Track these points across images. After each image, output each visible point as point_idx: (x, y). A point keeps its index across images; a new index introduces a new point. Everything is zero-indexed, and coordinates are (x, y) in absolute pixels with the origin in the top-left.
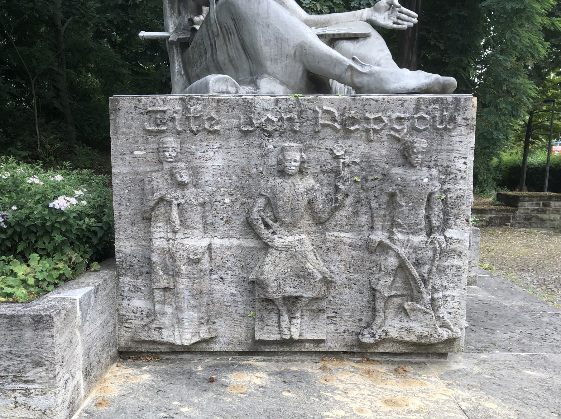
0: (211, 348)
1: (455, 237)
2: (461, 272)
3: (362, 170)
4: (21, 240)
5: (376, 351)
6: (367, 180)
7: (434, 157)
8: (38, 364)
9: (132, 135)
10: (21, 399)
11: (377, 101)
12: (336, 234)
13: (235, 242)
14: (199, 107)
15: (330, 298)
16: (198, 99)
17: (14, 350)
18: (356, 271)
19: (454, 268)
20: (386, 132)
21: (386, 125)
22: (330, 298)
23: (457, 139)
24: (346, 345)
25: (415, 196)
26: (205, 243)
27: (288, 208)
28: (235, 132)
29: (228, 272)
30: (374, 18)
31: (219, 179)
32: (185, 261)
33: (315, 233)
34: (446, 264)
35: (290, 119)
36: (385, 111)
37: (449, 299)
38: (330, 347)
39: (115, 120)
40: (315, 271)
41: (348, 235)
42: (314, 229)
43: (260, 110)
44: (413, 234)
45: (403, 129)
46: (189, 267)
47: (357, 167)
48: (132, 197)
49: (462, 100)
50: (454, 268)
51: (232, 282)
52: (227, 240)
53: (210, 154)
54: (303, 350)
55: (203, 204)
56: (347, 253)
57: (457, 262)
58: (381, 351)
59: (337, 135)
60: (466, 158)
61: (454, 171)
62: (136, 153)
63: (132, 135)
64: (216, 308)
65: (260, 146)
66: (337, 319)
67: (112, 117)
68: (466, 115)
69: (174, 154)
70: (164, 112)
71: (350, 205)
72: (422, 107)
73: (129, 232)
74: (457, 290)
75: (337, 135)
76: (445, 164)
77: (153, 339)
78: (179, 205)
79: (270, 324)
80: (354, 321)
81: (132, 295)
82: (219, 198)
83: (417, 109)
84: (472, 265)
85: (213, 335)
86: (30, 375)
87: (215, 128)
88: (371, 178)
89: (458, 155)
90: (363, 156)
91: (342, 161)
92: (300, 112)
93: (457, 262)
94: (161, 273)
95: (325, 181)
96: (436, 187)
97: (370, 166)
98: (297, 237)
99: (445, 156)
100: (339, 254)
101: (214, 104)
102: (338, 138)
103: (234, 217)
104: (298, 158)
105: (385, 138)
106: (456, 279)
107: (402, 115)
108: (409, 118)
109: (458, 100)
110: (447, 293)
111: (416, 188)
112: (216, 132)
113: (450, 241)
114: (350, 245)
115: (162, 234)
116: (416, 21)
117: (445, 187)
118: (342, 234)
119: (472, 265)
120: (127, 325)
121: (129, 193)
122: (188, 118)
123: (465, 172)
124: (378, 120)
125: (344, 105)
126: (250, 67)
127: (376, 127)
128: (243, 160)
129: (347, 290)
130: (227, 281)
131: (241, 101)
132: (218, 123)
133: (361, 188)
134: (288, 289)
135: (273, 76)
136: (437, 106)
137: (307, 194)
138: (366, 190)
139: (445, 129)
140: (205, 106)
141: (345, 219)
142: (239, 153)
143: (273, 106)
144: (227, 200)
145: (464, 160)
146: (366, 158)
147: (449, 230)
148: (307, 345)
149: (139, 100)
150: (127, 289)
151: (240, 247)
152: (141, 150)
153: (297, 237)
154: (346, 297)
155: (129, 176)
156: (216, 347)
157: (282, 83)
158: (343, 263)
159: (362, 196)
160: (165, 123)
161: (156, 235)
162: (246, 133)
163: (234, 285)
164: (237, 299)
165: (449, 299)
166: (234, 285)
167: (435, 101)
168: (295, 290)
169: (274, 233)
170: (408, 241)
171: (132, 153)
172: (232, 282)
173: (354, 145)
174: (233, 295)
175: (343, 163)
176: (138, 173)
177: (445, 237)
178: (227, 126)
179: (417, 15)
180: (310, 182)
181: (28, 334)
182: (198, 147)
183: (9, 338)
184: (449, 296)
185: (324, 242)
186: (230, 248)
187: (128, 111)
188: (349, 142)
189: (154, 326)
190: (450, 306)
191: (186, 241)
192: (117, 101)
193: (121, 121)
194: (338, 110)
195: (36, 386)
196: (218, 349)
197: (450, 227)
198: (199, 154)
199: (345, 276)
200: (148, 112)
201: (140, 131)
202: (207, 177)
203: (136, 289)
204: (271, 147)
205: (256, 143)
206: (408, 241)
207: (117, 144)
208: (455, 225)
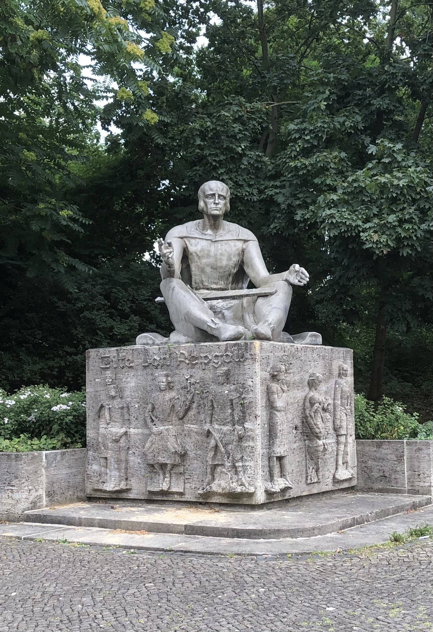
0: (129, 496)
1: (250, 427)
2: (254, 450)
3: (201, 387)
4: (43, 429)
5: (211, 501)
6: (203, 393)
7: (236, 379)
8: (16, 478)
9: (95, 371)
10: (10, 494)
11: (206, 346)
12: (189, 425)
13: (140, 430)
14: (124, 354)
15: (187, 466)
16: (124, 349)
17: (9, 470)
18: (199, 449)
19: (250, 447)
20: (211, 364)
21: (211, 360)
22: (187, 466)
23: (247, 367)
24: (196, 497)
25: (221, 401)
26: (123, 430)
27: (160, 410)
28: (140, 367)
29: (137, 449)
30: (288, 278)
31: (133, 394)
32: (111, 441)
33: (178, 425)
34: (246, 445)
35: (164, 359)
36: (210, 352)
37: (248, 468)
38: (188, 498)
39: (88, 363)
40: (171, 447)
41: (195, 426)
42: (178, 422)
43: (151, 354)
44: (223, 425)
45: (218, 362)
46: (113, 444)
47: (198, 385)
48: (94, 405)
49: (249, 344)
50: (250, 447)
51: (139, 455)
52: (136, 429)
53: (129, 379)
54: (174, 499)
55: (122, 408)
56: (195, 437)
57: (251, 444)
58: (214, 501)
59: (188, 367)
60: (252, 378)
61: (247, 386)
62: (97, 380)
63: (95, 371)
64: (131, 471)
65: (152, 374)
66: (191, 480)
67: (87, 361)
68: (251, 353)
69: (110, 380)
70: (109, 357)
71: (196, 408)
72: (229, 349)
73: (92, 425)
74: (253, 462)
75: (188, 367)
76: (242, 383)
77: (99, 488)
78: (109, 408)
79: (155, 481)
80: (199, 481)
81: (93, 462)
82: (133, 404)
83: (226, 350)
84: (426, 475)
85: (128, 487)
86: (13, 483)
87: (131, 365)
88: (205, 391)
89: (248, 377)
90: (201, 379)
91: (189, 381)
92: (170, 354)
93: (251, 444)
94: (103, 448)
95: (183, 394)
96: (234, 395)
97: (204, 384)
98: (166, 427)
99: (242, 377)
100: (191, 438)
101: (131, 352)
102: (188, 368)
103: (140, 416)
104: (164, 380)
105: (211, 368)
106: (251, 454)
107: (218, 354)
108: (222, 356)
109: (246, 344)
110: (247, 464)
111: (221, 397)
112: (131, 367)
113: (247, 430)
114: (196, 432)
115: (103, 426)
116: (308, 280)
117: (243, 396)
118: (192, 426)
119: (426, 475)
120: (91, 481)
121: (93, 403)
122: (119, 360)
123: (253, 386)
124: (206, 357)
125: (191, 349)
126: (166, 328)
127: (206, 362)
128: (144, 383)
129: (195, 461)
130: (136, 455)
131: (143, 350)
132: (133, 362)
133: (201, 398)
134: (160, 458)
135: (180, 332)
136: (236, 348)
137: (171, 401)
138: (203, 399)
139: (239, 361)
140: (127, 353)
141: (193, 417)
142: (142, 378)
143: (158, 351)
144: (137, 406)
145: (252, 380)
146: (202, 379)
147: (246, 423)
148: (176, 496)
149: (99, 352)
150: (91, 459)
151: (143, 434)
152: (99, 379)
153: (166, 427)
154: (195, 465)
155: (93, 393)
156: (131, 496)
157: (184, 335)
158: (193, 444)
159: (201, 402)
160: (109, 363)
161: (101, 426)
162: (145, 367)
163: (140, 457)
164: (141, 466)
165: (248, 468)
166: (140, 457)
167: (235, 345)
168: (163, 459)
169: (155, 425)
170: (221, 429)
171: (95, 380)
172: (139, 455)
173: (197, 372)
174: (139, 463)
175: (190, 383)
176: (97, 392)
177: (244, 427)
178: (137, 364)
179: (308, 276)
180: (173, 394)
181: (14, 463)
182: (124, 376)
183: (7, 465)
184: (248, 466)
185: (183, 431)
186: (138, 434)
187: (94, 357)
188: (194, 370)
189: (101, 481)
190: (249, 472)
191: (112, 429)
192: (89, 352)
193: (91, 363)
194: (188, 352)
195: (15, 488)
196: (132, 498)
197: (246, 422)
198: (124, 380)
199: (194, 452)
200: (102, 358)
201: (98, 369)
202: (127, 393)
203: (95, 459)
204: (157, 374)
205: (150, 372)
206: (221, 429)
207: (89, 376)
208: (249, 420)
